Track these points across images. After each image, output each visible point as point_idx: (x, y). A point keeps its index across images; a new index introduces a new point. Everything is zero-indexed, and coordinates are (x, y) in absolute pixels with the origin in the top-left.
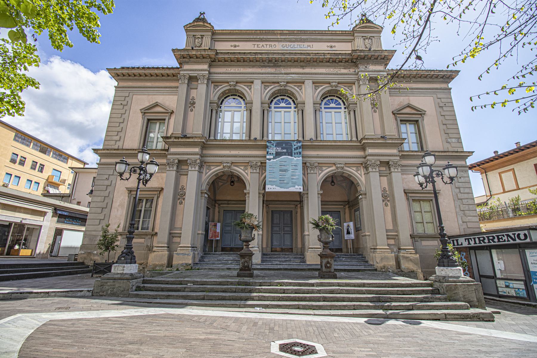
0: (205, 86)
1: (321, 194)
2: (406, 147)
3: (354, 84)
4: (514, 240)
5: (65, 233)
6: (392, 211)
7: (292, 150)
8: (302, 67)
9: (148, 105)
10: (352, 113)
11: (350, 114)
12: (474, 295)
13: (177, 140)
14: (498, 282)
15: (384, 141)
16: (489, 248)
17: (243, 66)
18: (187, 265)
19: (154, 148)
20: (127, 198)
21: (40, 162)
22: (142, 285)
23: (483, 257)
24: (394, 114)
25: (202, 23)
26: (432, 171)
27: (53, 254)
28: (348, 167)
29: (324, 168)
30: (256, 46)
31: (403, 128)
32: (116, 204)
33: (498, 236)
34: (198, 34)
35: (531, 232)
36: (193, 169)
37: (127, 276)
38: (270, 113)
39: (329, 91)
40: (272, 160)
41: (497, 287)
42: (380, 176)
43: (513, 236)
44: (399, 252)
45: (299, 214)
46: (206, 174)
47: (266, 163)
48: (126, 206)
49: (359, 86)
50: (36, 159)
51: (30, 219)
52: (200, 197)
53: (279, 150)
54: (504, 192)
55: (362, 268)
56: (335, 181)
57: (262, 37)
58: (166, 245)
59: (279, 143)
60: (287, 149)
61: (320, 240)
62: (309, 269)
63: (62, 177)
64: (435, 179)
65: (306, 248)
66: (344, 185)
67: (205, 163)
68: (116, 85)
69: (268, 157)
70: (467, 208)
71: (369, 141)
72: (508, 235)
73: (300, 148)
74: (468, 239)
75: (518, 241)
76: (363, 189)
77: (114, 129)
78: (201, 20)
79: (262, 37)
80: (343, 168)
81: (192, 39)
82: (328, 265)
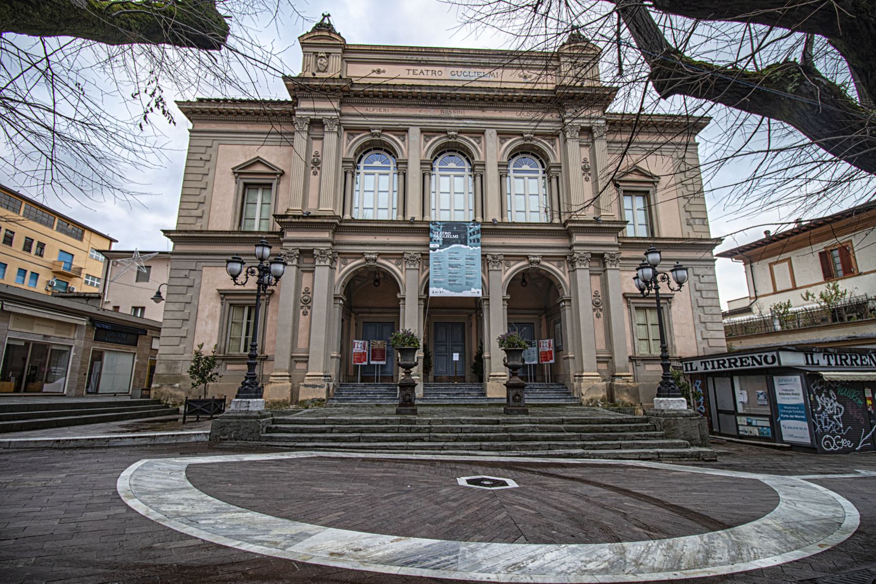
0: (335, 136)
1: (508, 301)
2: (629, 231)
3: (558, 136)
5: (106, 356)
6: (605, 323)
7: (466, 236)
8: (482, 108)
9: (244, 161)
10: (554, 181)
11: (550, 181)
12: (697, 431)
13: (297, 220)
14: (738, 418)
15: (597, 227)
16: (731, 374)
17: (392, 105)
19: (256, 229)
20: (220, 305)
21: (38, 238)
22: (274, 426)
23: (722, 386)
25: (327, 34)
26: (655, 274)
27: (90, 390)
28: (546, 261)
29: (512, 263)
30: (411, 72)
31: (627, 201)
32: (203, 314)
33: (741, 359)
34: (322, 51)
35: (781, 353)
37: (255, 414)
38: (433, 177)
39: (519, 147)
40: (438, 250)
41: (737, 426)
42: (591, 274)
43: (758, 359)
44: (613, 380)
45: (474, 328)
46: (341, 270)
47: (428, 255)
48: (218, 317)
49: (566, 140)
50: (32, 235)
51: (54, 337)
52: (332, 305)
53: (448, 235)
54: (775, 292)
55: (562, 402)
56: (527, 280)
57: (420, 58)
58: (287, 374)
59: (448, 226)
60: (459, 234)
61: (506, 365)
62: (490, 405)
63: (76, 264)
64: (660, 284)
65: (487, 376)
66: (540, 284)
67: (339, 254)
68: (191, 128)
69: (432, 246)
70: (709, 319)
71: (577, 225)
72: (753, 358)
73: (478, 233)
74: (705, 362)
75: (764, 365)
76: (566, 294)
77: (192, 199)
78: (324, 28)
79: (420, 58)
80: (538, 263)
81: (312, 59)
82: (517, 398)
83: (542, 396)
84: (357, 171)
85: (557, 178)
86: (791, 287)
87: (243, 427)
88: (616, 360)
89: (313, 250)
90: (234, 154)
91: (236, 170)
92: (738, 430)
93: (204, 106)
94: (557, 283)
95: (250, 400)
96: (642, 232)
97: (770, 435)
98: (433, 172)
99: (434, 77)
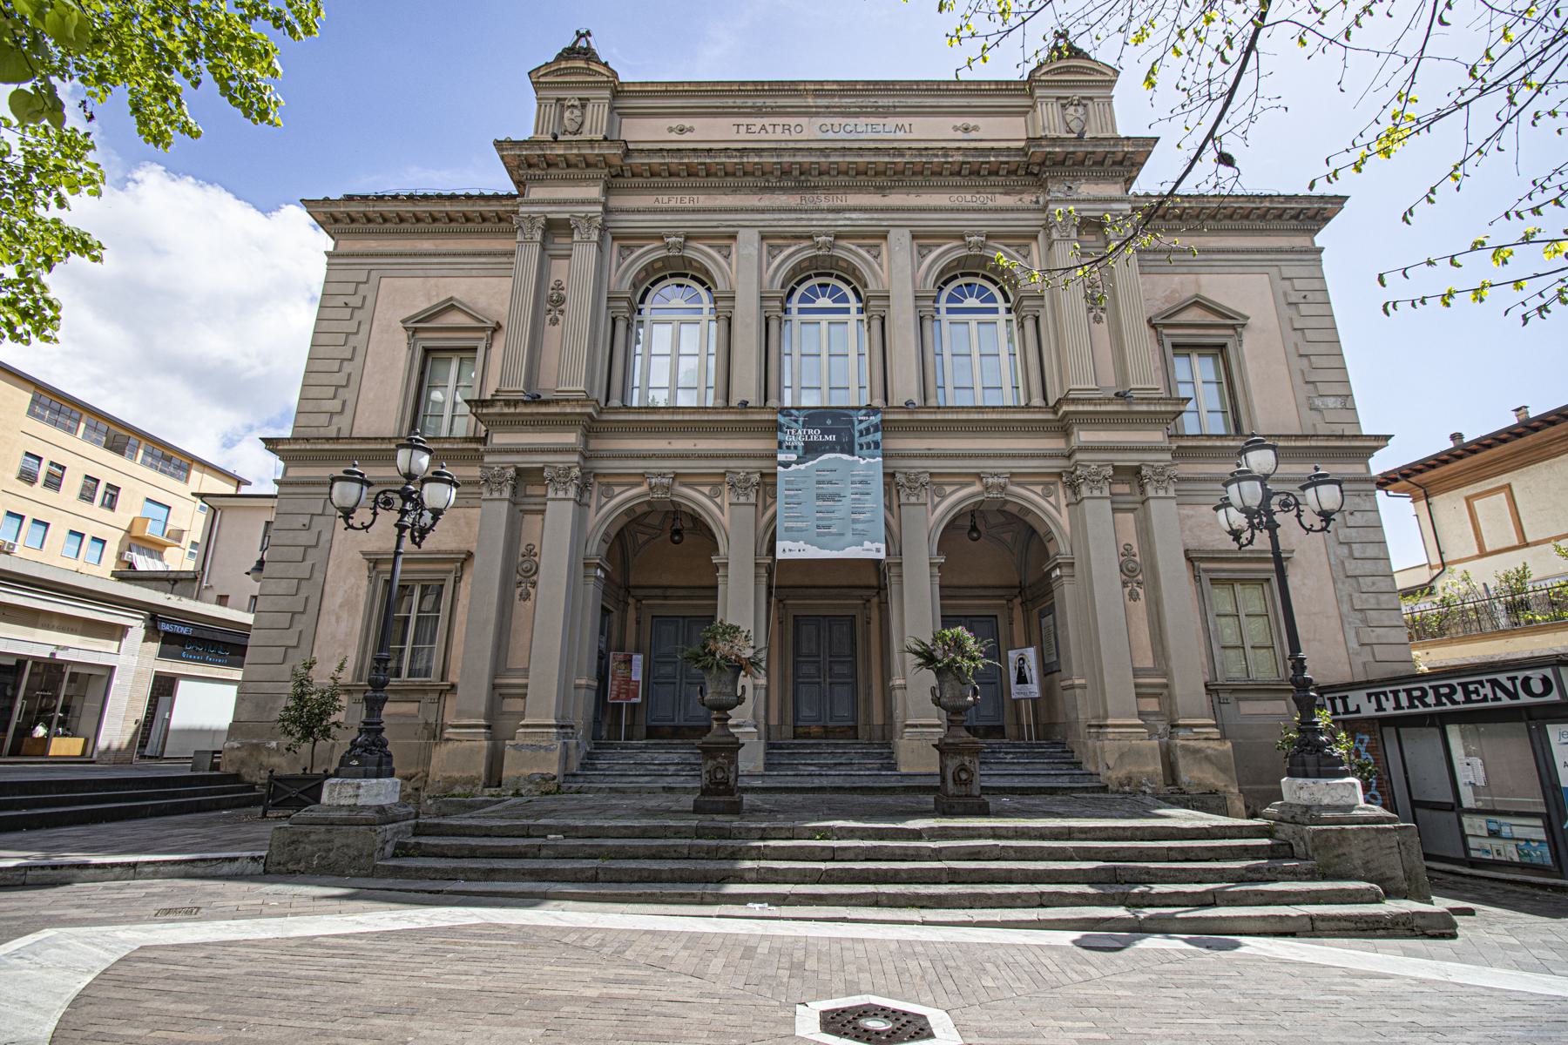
2: (1189, 424)
3: (1036, 238)
4: (1514, 696)
5: (183, 687)
8: (881, 190)
9: (425, 306)
11: (1022, 326)
13: (512, 410)
14: (1466, 820)
15: (1124, 409)
16: (1440, 721)
18: (546, 779)
19: (444, 433)
20: (365, 582)
21: (106, 477)
23: (1421, 749)
24: (1154, 327)
25: (581, 64)
26: (1268, 496)
27: (147, 752)
29: (948, 489)
30: (743, 129)
31: (1181, 367)
33: (1464, 686)
34: (572, 96)
36: (496, 495)
39: (959, 262)
40: (794, 467)
41: (1464, 837)
42: (1114, 510)
43: (1509, 685)
44: (1172, 736)
46: (600, 508)
48: (362, 608)
49: (1050, 246)
52: (581, 579)
53: (815, 435)
54: (1483, 554)
55: (1064, 782)
57: (759, 102)
58: (483, 722)
59: (815, 417)
60: (837, 432)
61: (937, 702)
62: (907, 790)
63: (174, 524)
65: (899, 725)
66: (1008, 537)
67: (596, 475)
68: (331, 249)
69: (781, 457)
70: (1372, 603)
72: (1495, 683)
73: (877, 430)
74: (1377, 695)
75: (1524, 699)
76: (1064, 548)
78: (579, 53)
79: (759, 102)
80: (1003, 488)
82: (964, 776)
83: (1019, 770)
84: (637, 317)
85: (1037, 319)
86: (1516, 543)
87: (338, 843)
88: (1178, 690)
89: (542, 469)
90: (406, 294)
91: (409, 325)
92: (1466, 849)
93: (354, 208)
94: (1041, 532)
95: (363, 782)
96: (1216, 425)
97: (1548, 861)
98: (788, 317)
99: (786, 136)
